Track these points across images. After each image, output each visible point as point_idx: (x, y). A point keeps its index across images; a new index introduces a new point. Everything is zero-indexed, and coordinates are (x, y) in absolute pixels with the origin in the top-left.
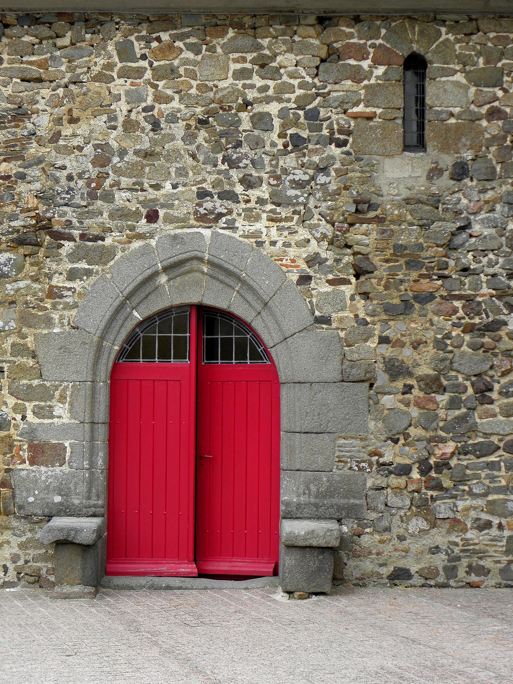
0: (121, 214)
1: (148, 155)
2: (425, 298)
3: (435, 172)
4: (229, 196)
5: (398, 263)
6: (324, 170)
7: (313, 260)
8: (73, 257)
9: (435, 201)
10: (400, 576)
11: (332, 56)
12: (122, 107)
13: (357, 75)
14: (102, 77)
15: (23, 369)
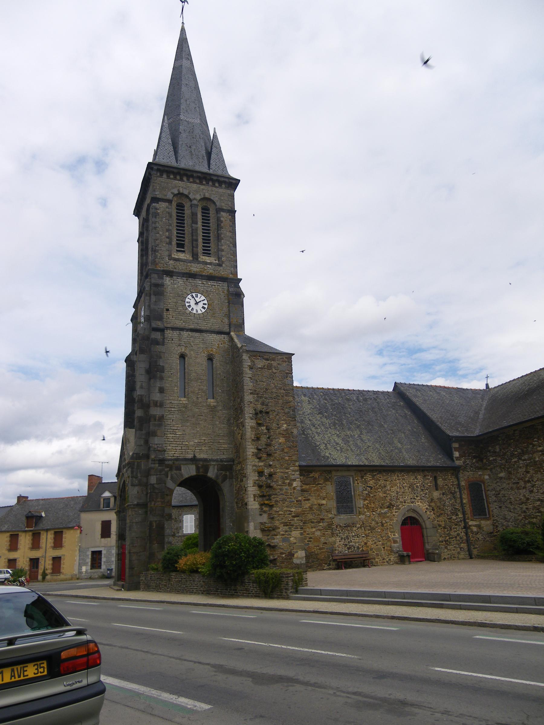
0: (401, 502)
1: (404, 492)
2: (442, 514)
3: (440, 494)
4: (414, 499)
5: (437, 508)
6: (426, 494)
7: (427, 509)
8: (396, 509)
9: (441, 499)
10: (445, 559)
11: (425, 476)
12: (398, 485)
13: (429, 479)
14: (395, 480)
15: (390, 528)
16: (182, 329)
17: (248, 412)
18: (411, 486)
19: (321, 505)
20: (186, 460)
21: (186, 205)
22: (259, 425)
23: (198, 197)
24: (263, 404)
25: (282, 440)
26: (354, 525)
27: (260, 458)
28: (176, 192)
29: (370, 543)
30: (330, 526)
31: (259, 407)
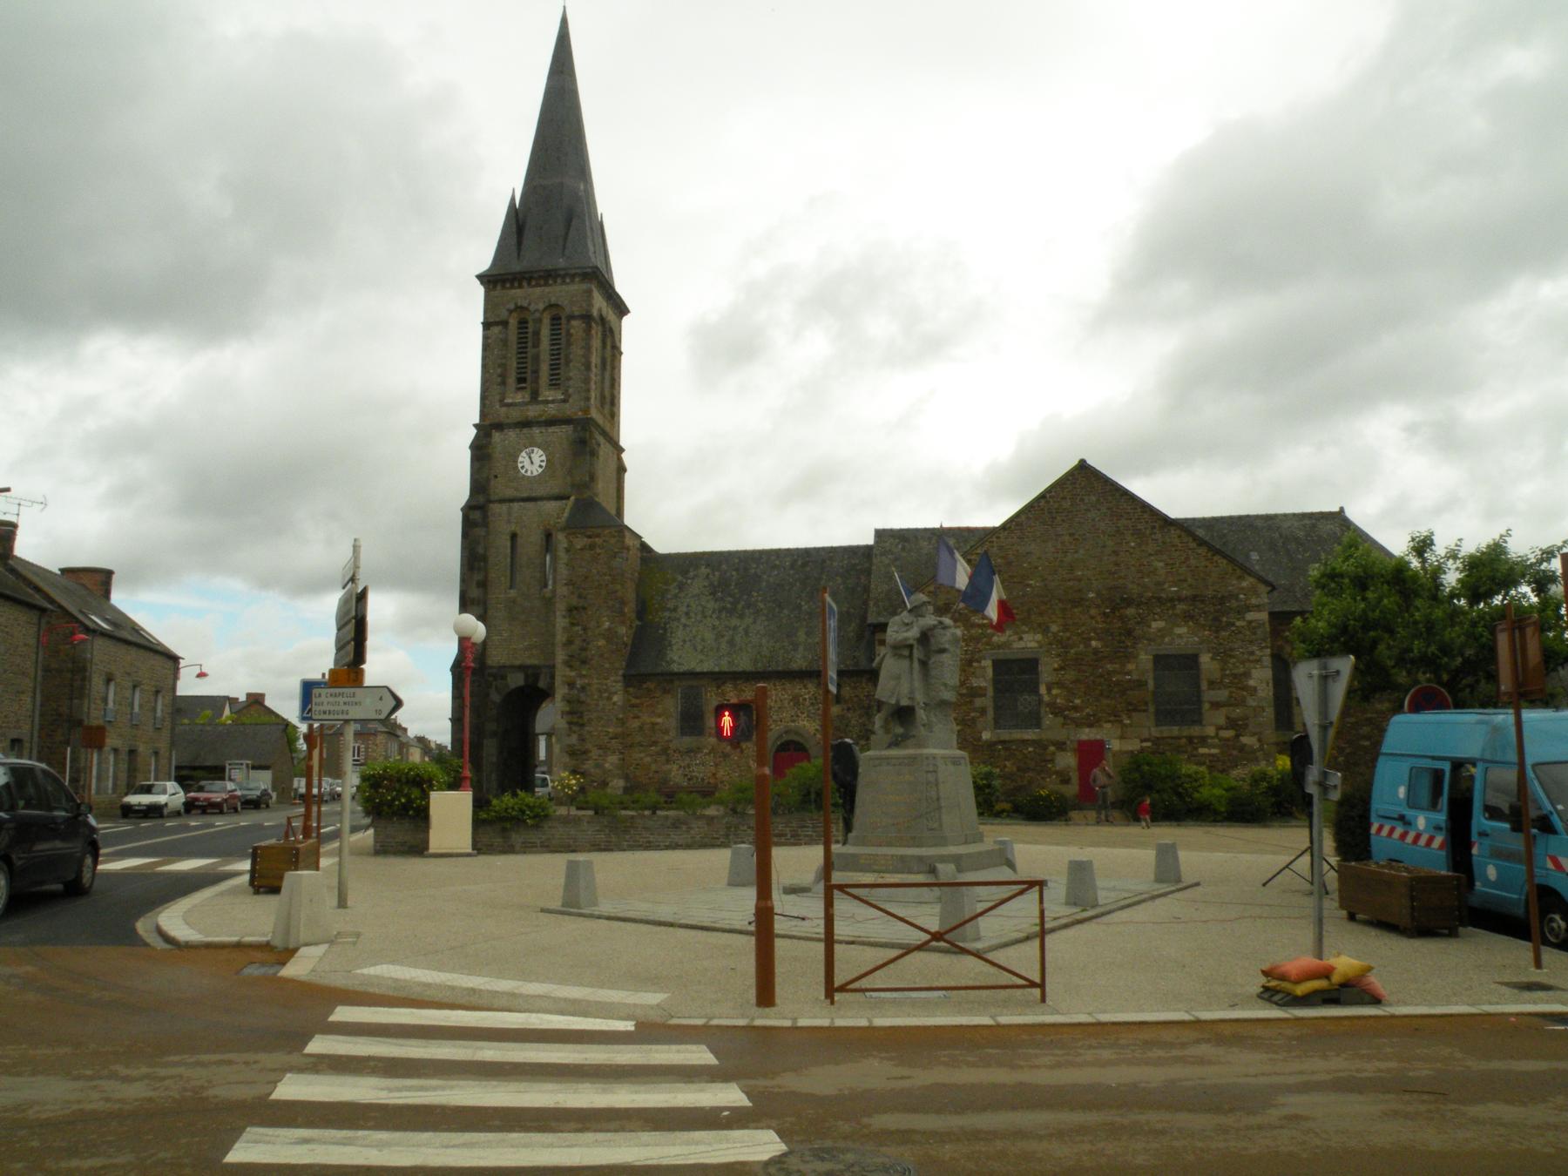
16: (512, 500)
17: (560, 607)
18: (795, 700)
19: (654, 724)
20: (512, 667)
21: (551, 299)
22: (573, 624)
23: (541, 306)
24: (580, 596)
25: (601, 643)
26: (699, 749)
27: (571, 667)
28: (512, 306)
29: (721, 773)
30: (665, 751)
31: (575, 601)
